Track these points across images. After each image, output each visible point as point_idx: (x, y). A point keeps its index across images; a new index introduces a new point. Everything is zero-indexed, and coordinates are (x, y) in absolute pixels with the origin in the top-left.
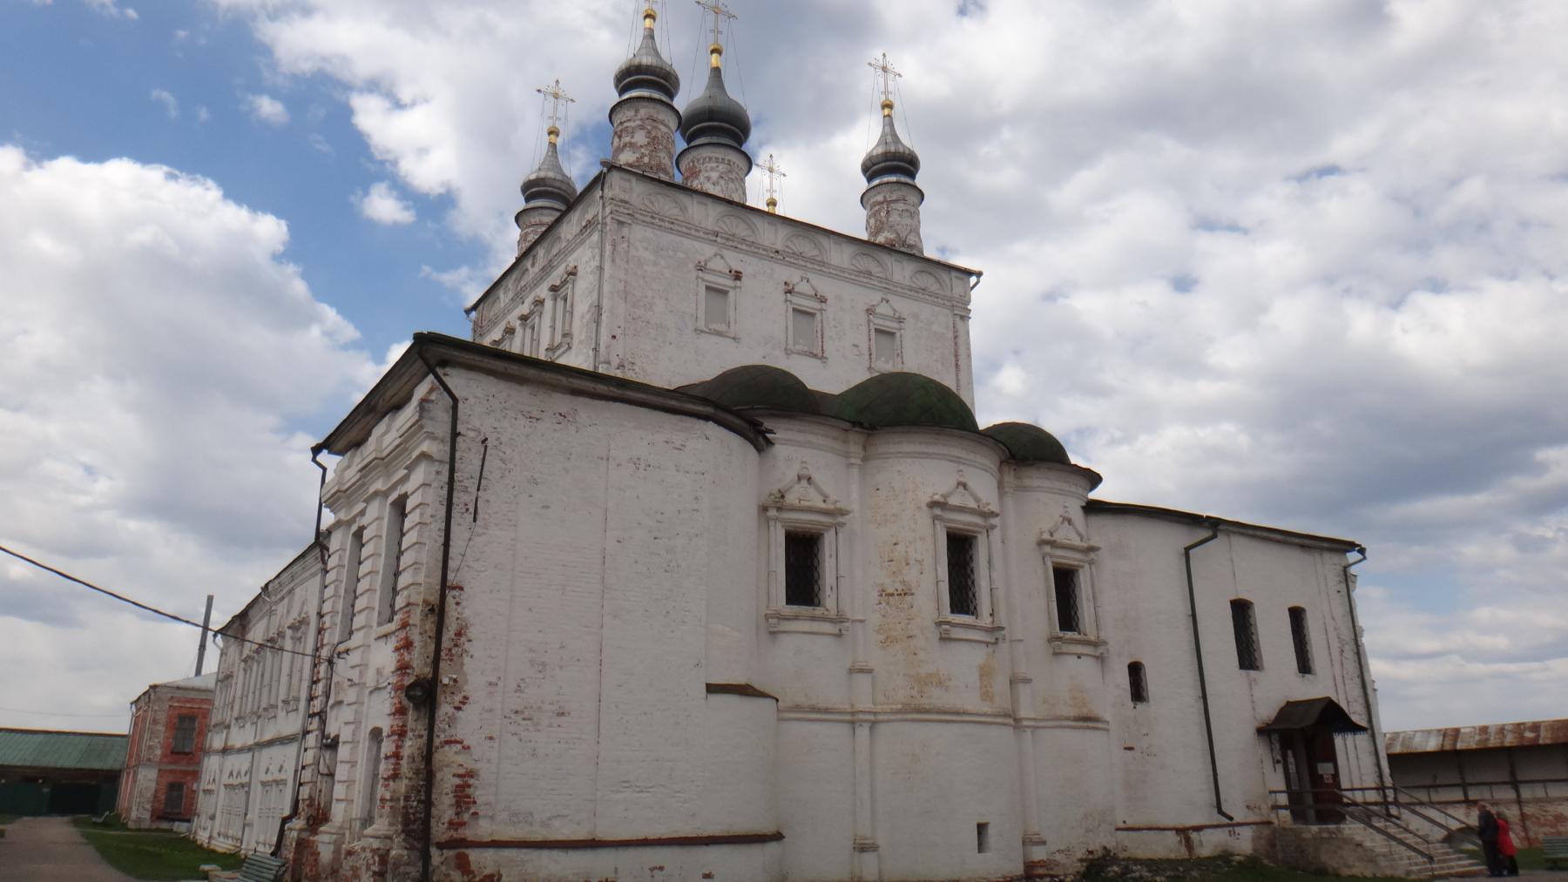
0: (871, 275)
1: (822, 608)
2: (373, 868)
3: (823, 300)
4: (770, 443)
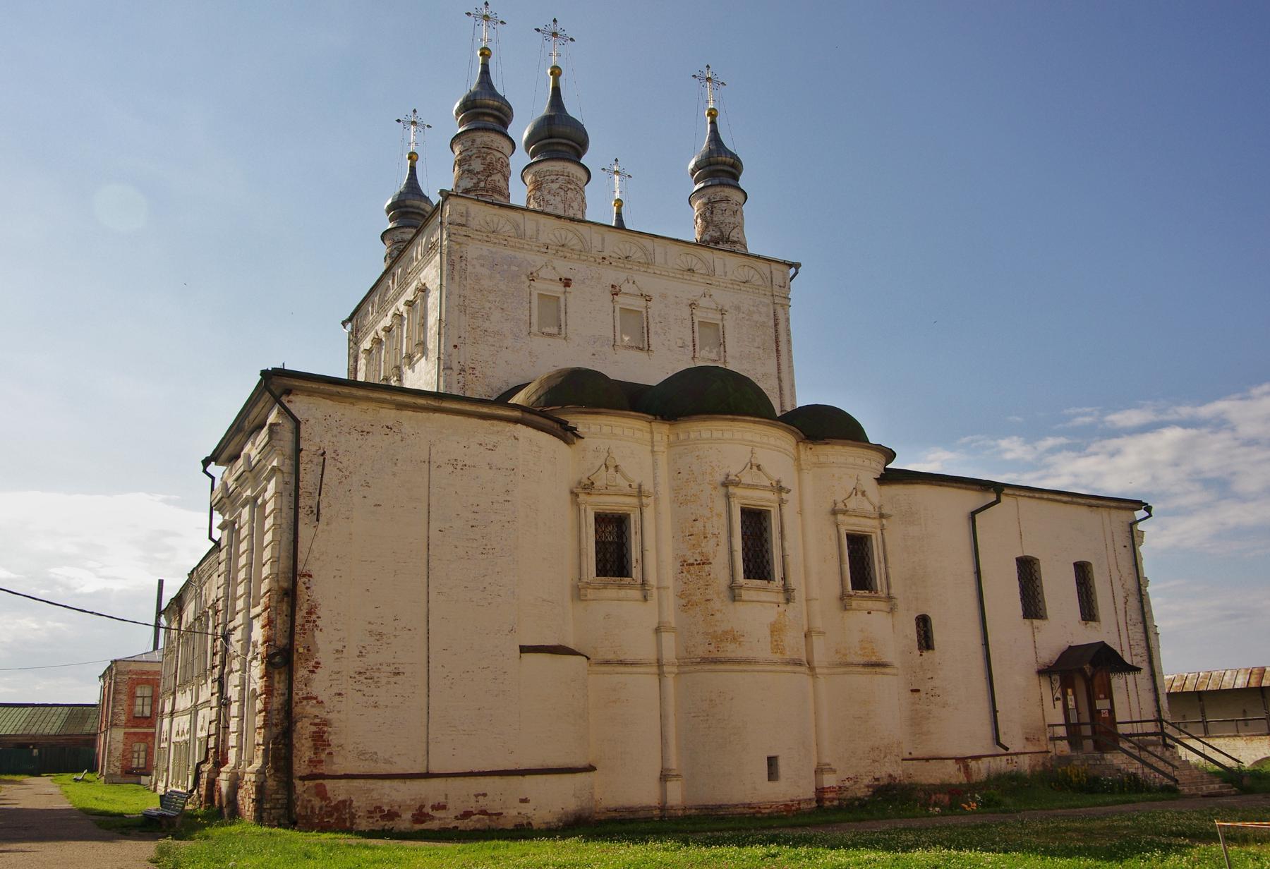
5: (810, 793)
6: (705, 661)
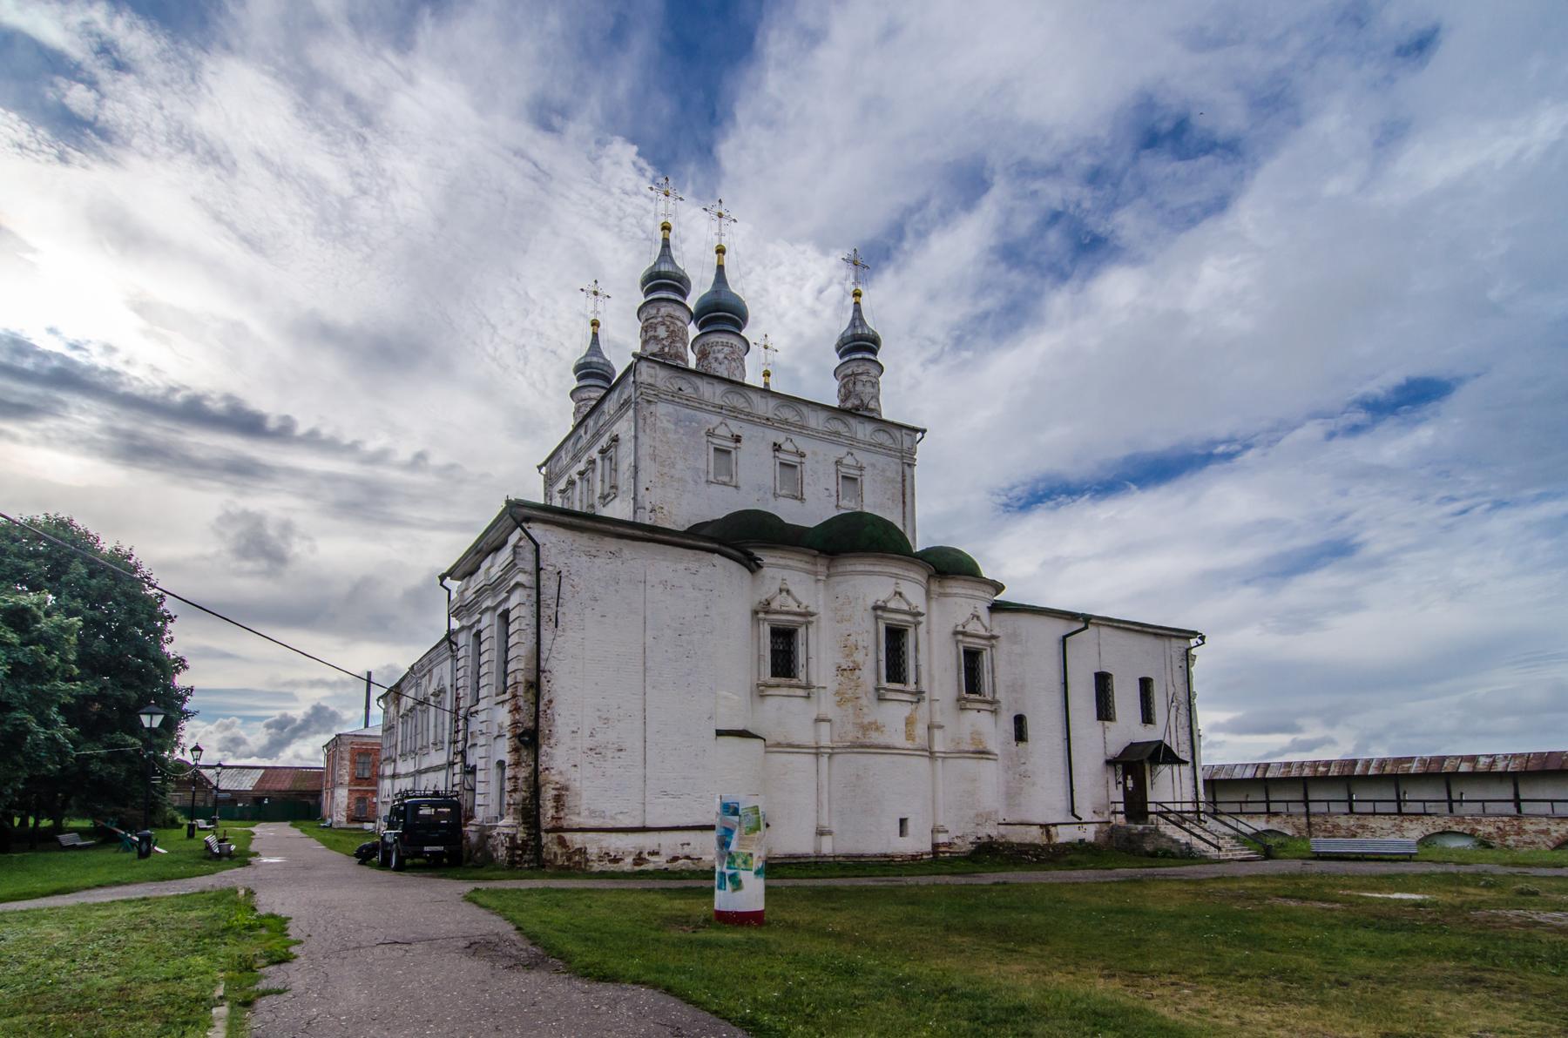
3: (802, 455)
4: (760, 567)
5: (929, 848)
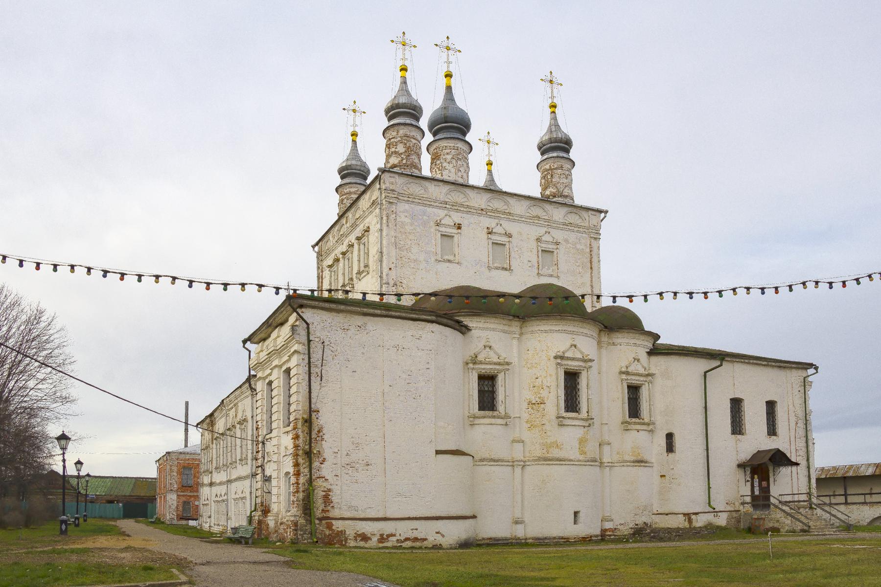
0: (539, 218)
1: (497, 412)
2: (292, 528)
3: (510, 236)
5: (598, 532)
6: (539, 459)
